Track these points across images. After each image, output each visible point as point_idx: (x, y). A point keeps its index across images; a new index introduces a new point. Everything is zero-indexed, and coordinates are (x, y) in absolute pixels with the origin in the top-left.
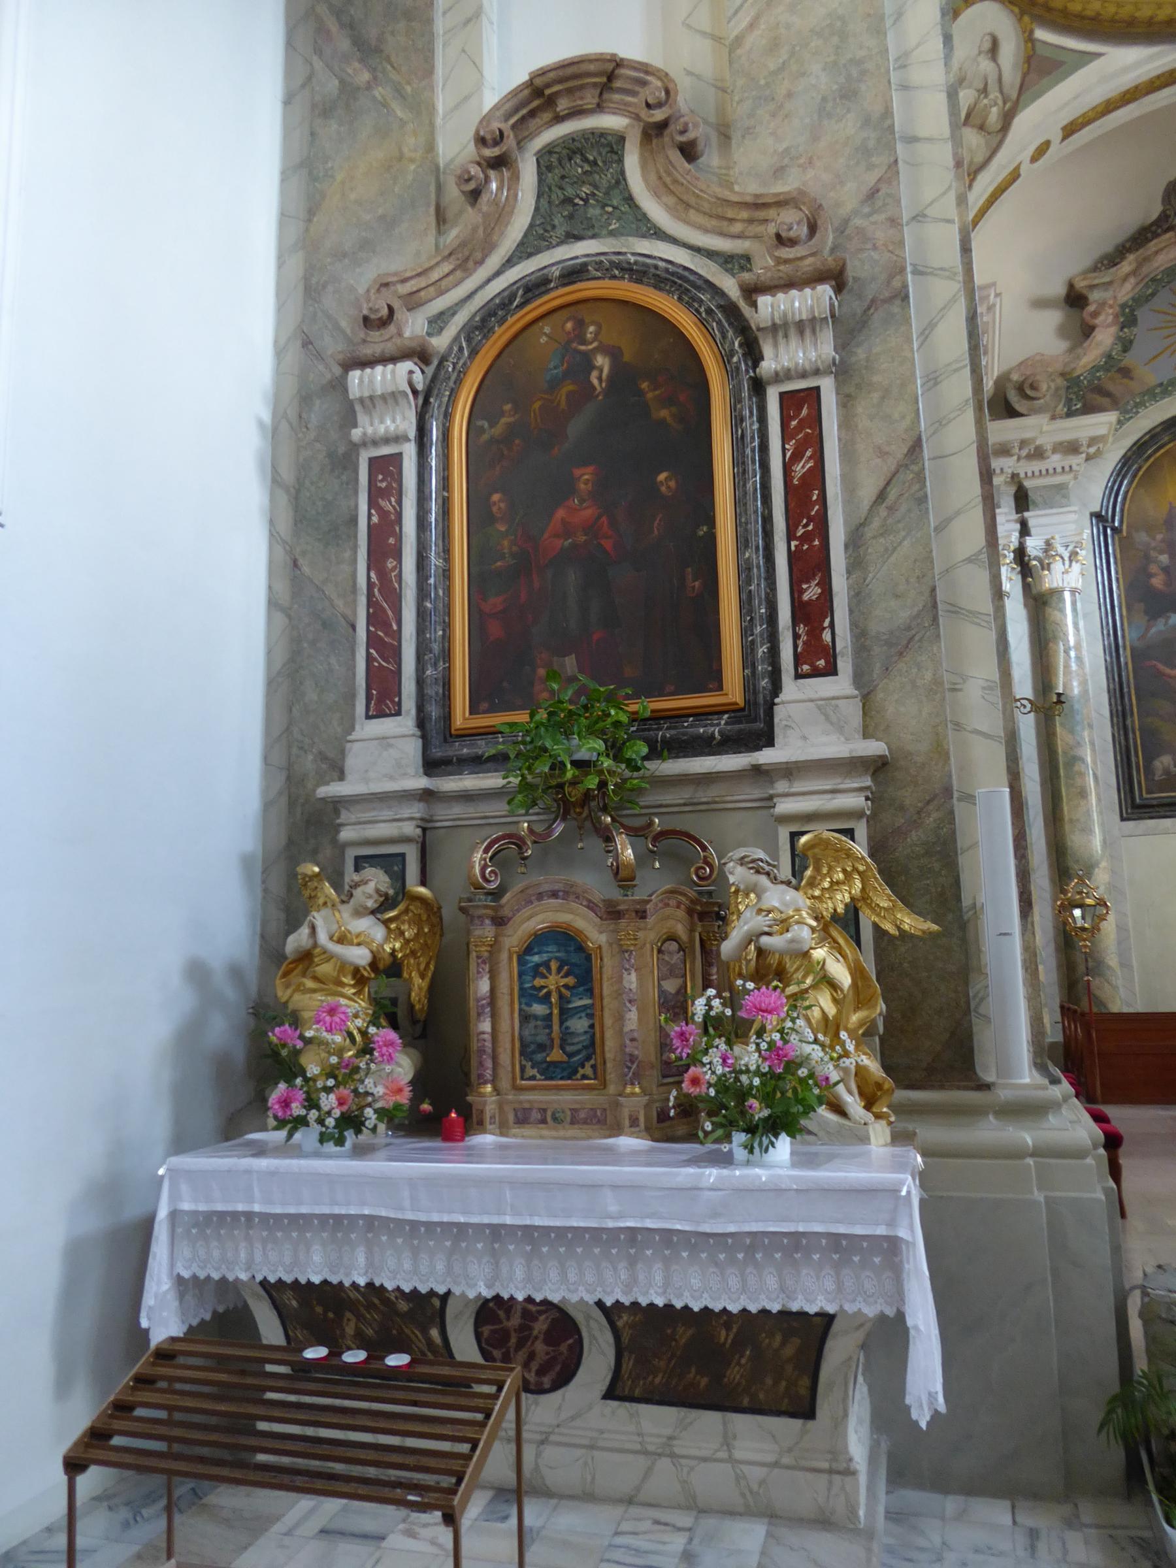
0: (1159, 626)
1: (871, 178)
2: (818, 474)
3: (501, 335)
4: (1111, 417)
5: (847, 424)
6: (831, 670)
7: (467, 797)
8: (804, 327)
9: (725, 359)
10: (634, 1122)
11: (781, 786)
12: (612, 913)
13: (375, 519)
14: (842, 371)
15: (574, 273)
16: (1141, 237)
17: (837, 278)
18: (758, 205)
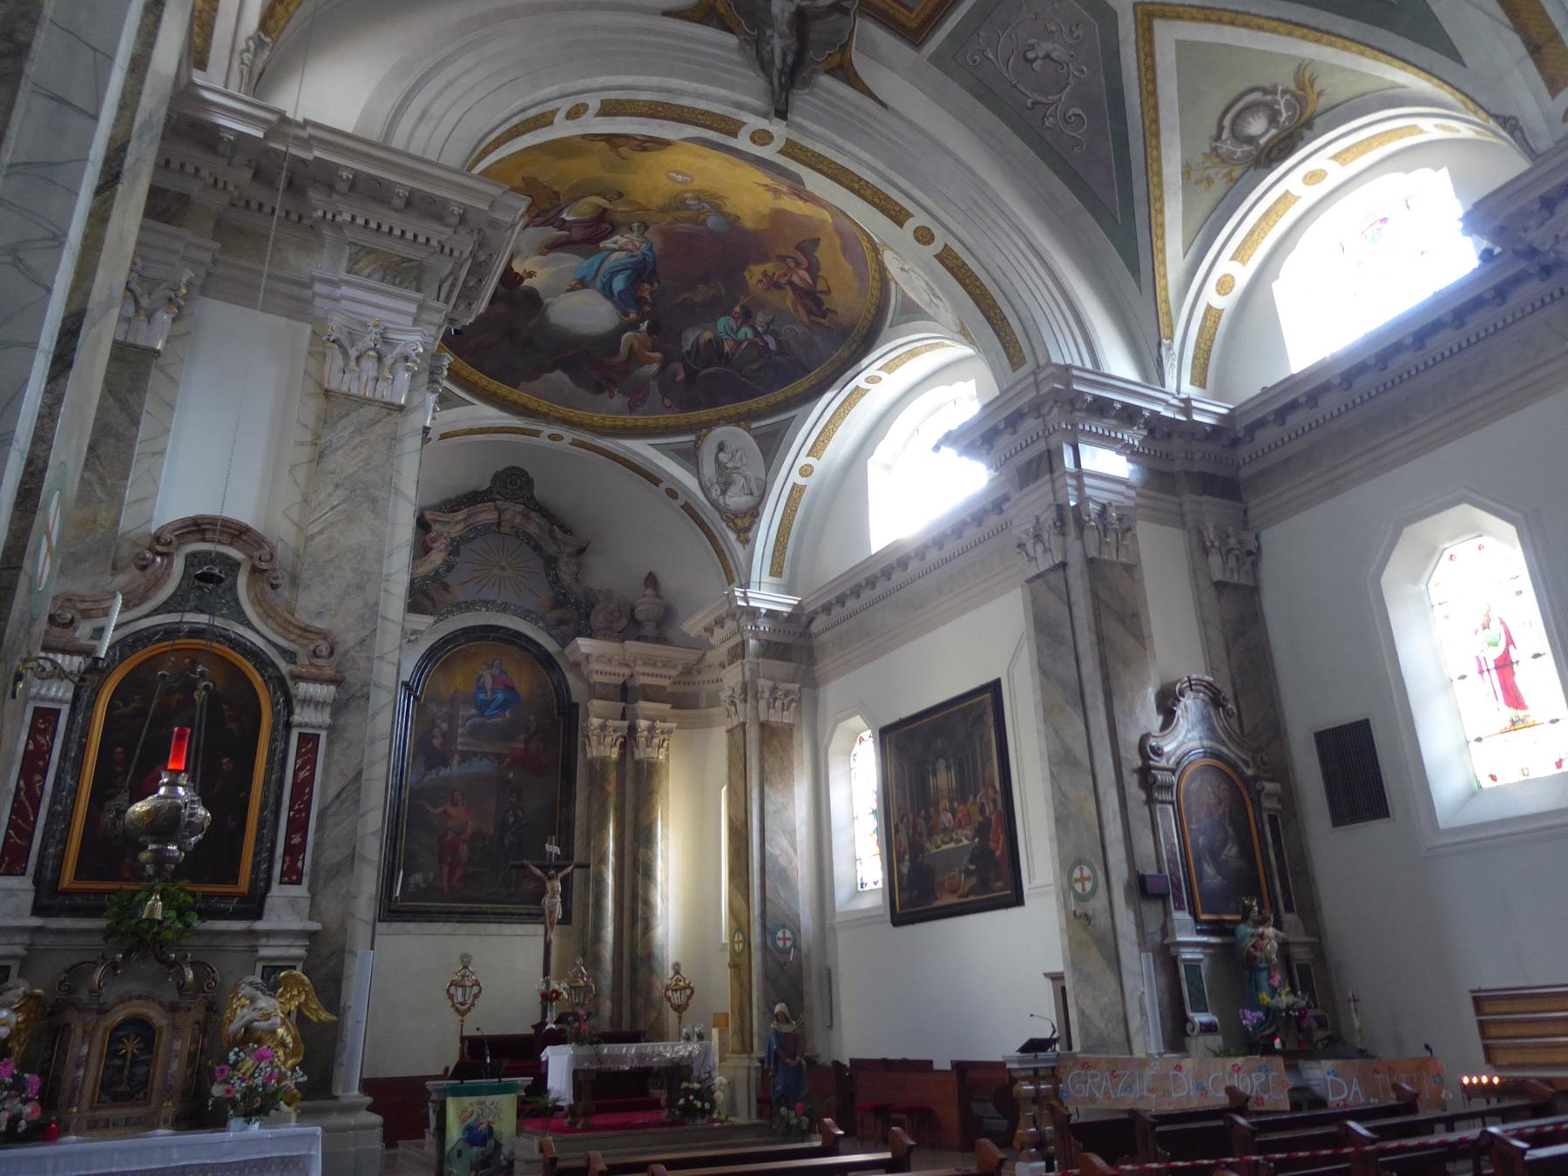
0: (432, 775)
1: (364, 633)
2: (310, 780)
3: (142, 654)
4: (429, 619)
5: (328, 755)
6: (299, 882)
7: (62, 932)
8: (318, 704)
9: (274, 704)
10: (166, 1122)
11: (263, 941)
12: (173, 1008)
13: (31, 747)
14: (331, 729)
15: (196, 632)
16: (472, 499)
17: (336, 681)
18: (306, 629)
